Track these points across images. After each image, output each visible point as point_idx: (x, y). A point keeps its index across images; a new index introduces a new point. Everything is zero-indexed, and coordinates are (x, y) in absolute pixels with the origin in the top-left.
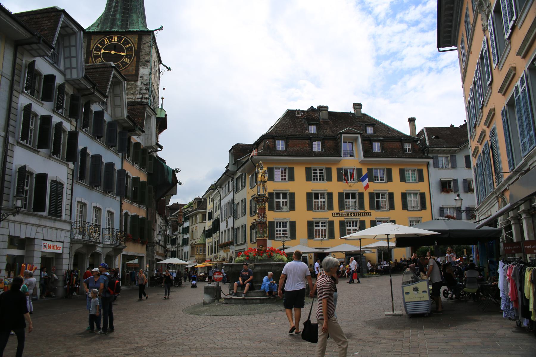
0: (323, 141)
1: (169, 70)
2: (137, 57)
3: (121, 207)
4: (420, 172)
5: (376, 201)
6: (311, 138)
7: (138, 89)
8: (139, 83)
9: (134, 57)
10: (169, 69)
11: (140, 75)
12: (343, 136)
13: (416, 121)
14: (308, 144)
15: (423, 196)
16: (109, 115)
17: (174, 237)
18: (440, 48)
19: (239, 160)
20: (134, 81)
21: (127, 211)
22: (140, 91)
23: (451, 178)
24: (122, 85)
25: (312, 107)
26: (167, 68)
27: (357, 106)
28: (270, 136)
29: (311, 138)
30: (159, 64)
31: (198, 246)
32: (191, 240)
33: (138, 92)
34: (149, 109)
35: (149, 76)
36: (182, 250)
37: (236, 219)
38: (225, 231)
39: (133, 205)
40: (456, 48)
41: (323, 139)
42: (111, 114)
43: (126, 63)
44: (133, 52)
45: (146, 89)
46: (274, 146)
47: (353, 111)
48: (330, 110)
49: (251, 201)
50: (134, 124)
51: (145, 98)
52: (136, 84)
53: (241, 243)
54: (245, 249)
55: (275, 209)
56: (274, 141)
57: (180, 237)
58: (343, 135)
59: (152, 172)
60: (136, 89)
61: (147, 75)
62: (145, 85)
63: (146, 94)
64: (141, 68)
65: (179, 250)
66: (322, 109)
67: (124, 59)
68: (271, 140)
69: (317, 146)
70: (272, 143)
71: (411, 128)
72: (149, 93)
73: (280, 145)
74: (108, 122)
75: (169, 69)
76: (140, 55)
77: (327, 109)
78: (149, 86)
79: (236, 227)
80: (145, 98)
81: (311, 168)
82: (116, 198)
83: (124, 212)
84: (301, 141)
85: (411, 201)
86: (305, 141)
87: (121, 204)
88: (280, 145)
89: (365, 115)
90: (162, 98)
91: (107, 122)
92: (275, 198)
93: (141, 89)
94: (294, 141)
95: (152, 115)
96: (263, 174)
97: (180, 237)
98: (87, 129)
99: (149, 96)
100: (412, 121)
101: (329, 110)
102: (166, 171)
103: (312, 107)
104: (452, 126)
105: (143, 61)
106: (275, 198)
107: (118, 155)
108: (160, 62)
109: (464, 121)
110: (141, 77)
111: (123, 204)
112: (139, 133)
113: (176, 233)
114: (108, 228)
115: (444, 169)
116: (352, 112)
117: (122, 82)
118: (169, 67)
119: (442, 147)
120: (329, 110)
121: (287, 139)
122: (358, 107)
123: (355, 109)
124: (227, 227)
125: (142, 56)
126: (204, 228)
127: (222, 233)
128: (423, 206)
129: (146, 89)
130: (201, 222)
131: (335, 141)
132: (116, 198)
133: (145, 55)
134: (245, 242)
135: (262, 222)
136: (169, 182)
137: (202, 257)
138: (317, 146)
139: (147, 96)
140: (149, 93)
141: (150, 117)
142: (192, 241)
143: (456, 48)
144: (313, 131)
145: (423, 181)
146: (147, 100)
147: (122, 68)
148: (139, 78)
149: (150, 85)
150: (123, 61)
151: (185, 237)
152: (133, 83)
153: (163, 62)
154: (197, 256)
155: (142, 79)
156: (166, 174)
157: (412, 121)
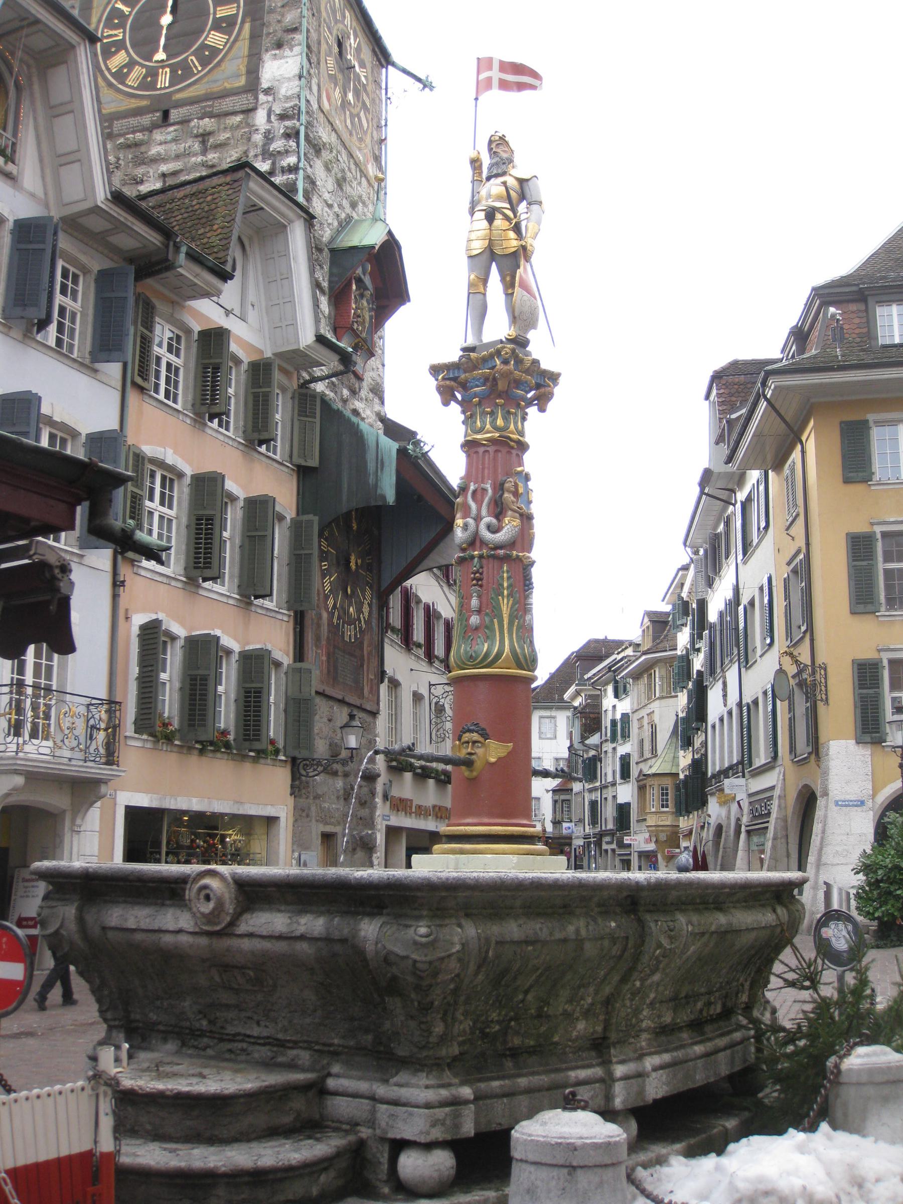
1: (425, 86)
2: (253, 20)
3: (115, 597)
7: (258, 138)
8: (260, 118)
9: (243, 22)
10: (426, 85)
11: (265, 85)
16: (32, 195)
17: (592, 753)
19: (734, 416)
20: (243, 112)
21: (161, 616)
22: (264, 145)
24: (76, 62)
26: (419, 80)
28: (847, 289)
30: (383, 66)
31: (656, 782)
32: (637, 763)
33: (259, 151)
34: (256, 182)
35: (297, 82)
36: (615, 797)
37: (747, 669)
38: (721, 720)
39: (201, 592)
42: (40, 193)
43: (215, 51)
44: (238, 7)
45: (287, 136)
46: (865, 330)
49: (786, 582)
50: (167, 233)
51: (283, 171)
52: (250, 121)
54: (772, 788)
55: (883, 608)
56: (867, 311)
57: (606, 752)
59: (314, 462)
60: (249, 139)
61: (289, 79)
62: (283, 117)
63: (287, 152)
64: (267, 57)
65: (606, 799)
67: (207, 36)
68: (853, 307)
70: (857, 321)
72: (298, 146)
74: (17, 222)
75: (426, 85)
76: (263, 8)
78: (299, 120)
79: (747, 699)
80: (283, 171)
82: (82, 556)
83: (139, 619)
87: (117, 584)
90: (872, 524)
91: (11, 220)
92: (880, 558)
93: (269, 137)
95: (291, 222)
96: (498, 204)
97: (606, 752)
98: (228, 417)
99: (299, 161)
102: (371, 456)
105: (275, 31)
106: (880, 558)
107: (96, 371)
108: (382, 56)
110: (268, 91)
111: (123, 583)
112: (207, 283)
113: (594, 740)
114: (12, 685)
117: (73, 47)
118: (423, 77)
124: (725, 705)
125: (271, 11)
126: (675, 718)
127: (714, 727)
129: (287, 136)
130: (664, 694)
132: (82, 556)
133: (283, 6)
134: (775, 757)
135: (483, 543)
136: (383, 497)
137: (668, 823)
139: (292, 160)
140: (298, 146)
141: (285, 227)
142: (642, 766)
146: (292, 176)
147: (199, 72)
148: (262, 97)
149: (303, 118)
150: (204, 47)
151: (622, 750)
152: (238, 118)
153: (395, 56)
154: (651, 821)
155: (270, 98)
156: (371, 466)
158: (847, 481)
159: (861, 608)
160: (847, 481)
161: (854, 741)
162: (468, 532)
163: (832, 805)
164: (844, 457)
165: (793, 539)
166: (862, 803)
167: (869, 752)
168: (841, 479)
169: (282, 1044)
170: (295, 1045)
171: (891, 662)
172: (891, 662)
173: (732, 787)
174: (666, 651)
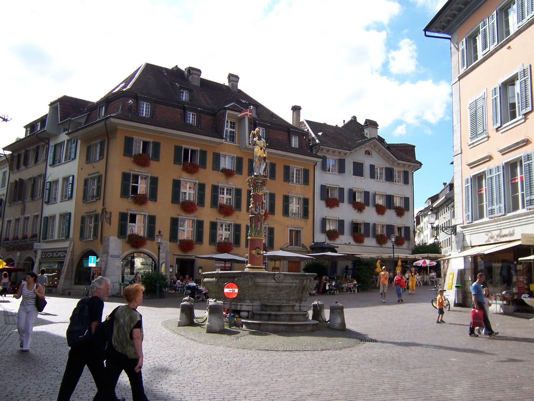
0: (199, 114)
4: (306, 172)
5: (132, 185)
6: (184, 108)
12: (228, 113)
13: (301, 111)
14: (180, 114)
15: (306, 202)
18: (426, 32)
23: (384, 193)
25: (177, 66)
27: (233, 78)
28: (132, 94)
29: (184, 108)
40: (450, 37)
41: (201, 112)
47: (227, 84)
48: (203, 76)
53: (56, 238)
58: (228, 112)
66: (194, 72)
69: (191, 118)
71: (295, 117)
73: (145, 109)
75: (454, 156)
77: (199, 73)
81: (182, 147)
84: (171, 108)
85: (185, 193)
86: (177, 109)
88: (145, 109)
89: (240, 91)
92: (131, 182)
94: (163, 107)
100: (296, 109)
101: (201, 77)
103: (177, 66)
104: (337, 126)
109: (343, 121)
115: (331, 174)
116: (225, 84)
119: (334, 147)
120: (201, 77)
121: (154, 102)
122: (235, 79)
123: (230, 81)
128: (305, 214)
131: (214, 117)
138: (191, 118)
143: (450, 37)
144: (184, 99)
145: (308, 185)
157: (296, 109)
158: (125, 155)
159: (305, 217)
160: (125, 155)
161: (117, 237)
162: (37, 145)
163: (109, 256)
164: (125, 148)
165: (94, 167)
166: (119, 257)
167: (121, 241)
168: (123, 154)
169: (281, 300)
170: (283, 300)
171: (131, 214)
172: (131, 214)
173: (37, 246)
174: (383, 230)
